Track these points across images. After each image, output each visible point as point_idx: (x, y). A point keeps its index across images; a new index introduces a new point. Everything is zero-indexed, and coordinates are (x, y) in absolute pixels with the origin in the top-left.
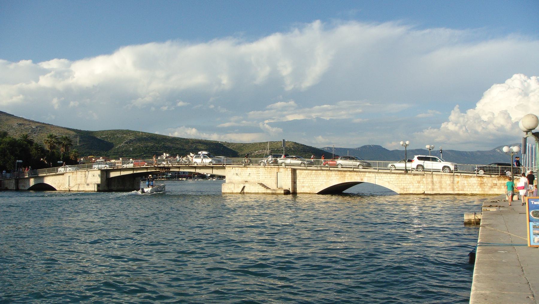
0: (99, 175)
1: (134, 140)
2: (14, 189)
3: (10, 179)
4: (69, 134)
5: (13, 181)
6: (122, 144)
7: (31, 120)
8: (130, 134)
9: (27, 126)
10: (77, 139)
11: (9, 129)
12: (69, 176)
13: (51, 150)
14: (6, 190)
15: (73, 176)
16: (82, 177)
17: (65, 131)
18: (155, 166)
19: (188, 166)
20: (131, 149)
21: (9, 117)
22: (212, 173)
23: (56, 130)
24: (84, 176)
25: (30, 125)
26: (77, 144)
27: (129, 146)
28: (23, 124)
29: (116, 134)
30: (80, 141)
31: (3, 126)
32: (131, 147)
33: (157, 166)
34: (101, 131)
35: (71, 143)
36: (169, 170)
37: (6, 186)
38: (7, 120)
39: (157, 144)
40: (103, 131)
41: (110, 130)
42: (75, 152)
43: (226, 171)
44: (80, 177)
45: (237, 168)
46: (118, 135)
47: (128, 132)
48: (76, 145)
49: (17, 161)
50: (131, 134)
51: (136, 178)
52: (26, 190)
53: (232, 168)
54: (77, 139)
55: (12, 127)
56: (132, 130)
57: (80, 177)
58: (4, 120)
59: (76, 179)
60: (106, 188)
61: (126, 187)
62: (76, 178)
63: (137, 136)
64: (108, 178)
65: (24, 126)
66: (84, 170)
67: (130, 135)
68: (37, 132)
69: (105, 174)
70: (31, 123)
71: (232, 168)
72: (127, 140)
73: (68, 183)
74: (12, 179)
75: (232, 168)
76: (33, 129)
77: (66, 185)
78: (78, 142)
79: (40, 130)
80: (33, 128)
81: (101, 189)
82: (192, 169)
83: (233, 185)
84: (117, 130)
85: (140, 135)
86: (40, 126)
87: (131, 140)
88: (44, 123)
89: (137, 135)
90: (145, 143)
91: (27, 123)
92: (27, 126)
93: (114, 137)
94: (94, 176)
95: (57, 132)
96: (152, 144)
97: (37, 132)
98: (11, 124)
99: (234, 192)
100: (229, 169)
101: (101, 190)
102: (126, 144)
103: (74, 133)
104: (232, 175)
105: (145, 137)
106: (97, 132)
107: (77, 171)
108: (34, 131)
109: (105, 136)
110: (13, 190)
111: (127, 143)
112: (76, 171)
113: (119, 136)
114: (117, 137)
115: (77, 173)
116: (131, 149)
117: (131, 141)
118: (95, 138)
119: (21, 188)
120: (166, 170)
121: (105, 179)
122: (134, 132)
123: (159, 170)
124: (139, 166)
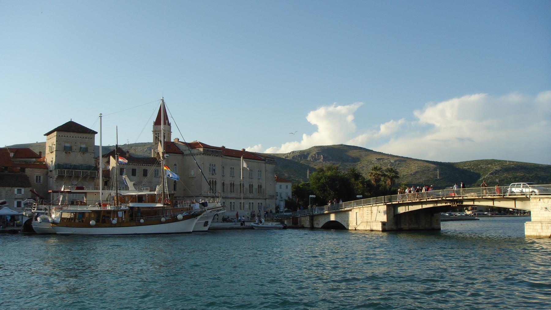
0: (384, 212)
1: (501, 170)
2: (309, 227)
3: (306, 216)
4: (429, 167)
5: (308, 218)
6: (487, 176)
7: (390, 154)
8: (495, 164)
9: (386, 161)
10: (437, 172)
11: (368, 165)
12: (356, 213)
13: (376, 183)
14: (303, 228)
15: (360, 212)
16: (369, 214)
17: (424, 164)
18: (443, 198)
19: (481, 197)
20: (497, 180)
21: (368, 152)
22: (514, 207)
23: (415, 163)
24: (370, 212)
25: (389, 160)
26: (437, 177)
27: (495, 178)
28: (382, 159)
29: (479, 165)
30: (440, 174)
31: (363, 162)
32: (497, 179)
33: (445, 199)
34: (462, 162)
35: (398, 175)
36: (462, 203)
37: (302, 224)
38: (366, 155)
39: (528, 174)
40: (465, 162)
41: (473, 161)
42: (405, 185)
43: (531, 203)
44: (367, 214)
45: (546, 200)
46: (482, 166)
47: (493, 162)
48: (436, 178)
49: (310, 196)
50: (496, 164)
51: (435, 215)
52: (190, 233)
53: (540, 200)
54: (437, 172)
55: (371, 162)
56: (497, 159)
57: (367, 214)
58: (363, 156)
59: (363, 217)
60: (394, 227)
61: (420, 226)
62: (363, 215)
63: (504, 166)
64: (395, 214)
65: (383, 161)
66: (370, 205)
67: (495, 165)
68: (396, 166)
69: (393, 209)
70: (390, 157)
71: (538, 199)
72: (492, 170)
73: (356, 221)
74: (307, 216)
75: (540, 200)
76: (392, 163)
77: (354, 223)
78: (438, 175)
79: (398, 164)
80: (392, 162)
81: (387, 228)
82: (470, 202)
83: (540, 224)
84: (481, 160)
85: (506, 165)
86: (398, 160)
87: (496, 170)
88: (402, 157)
89: (504, 164)
90: (513, 173)
91: (385, 157)
92: (386, 161)
93: (478, 168)
94: (546, 208)
95: (416, 165)
96: (522, 175)
97: (396, 166)
98: (370, 160)
99: (541, 235)
100: (535, 201)
101: (387, 229)
102: (491, 176)
103: (434, 166)
104: (540, 210)
105: (513, 167)
106: (458, 164)
107: (364, 206)
108: (393, 165)
109: (467, 168)
110: (308, 228)
111: (492, 174)
112: (362, 206)
113: (484, 166)
114: (481, 168)
115: (363, 209)
116: (497, 180)
117: (497, 172)
118: (458, 170)
119: (316, 226)
120: (458, 204)
121: (393, 215)
122: (499, 161)
123: (450, 204)
124: (411, 200)
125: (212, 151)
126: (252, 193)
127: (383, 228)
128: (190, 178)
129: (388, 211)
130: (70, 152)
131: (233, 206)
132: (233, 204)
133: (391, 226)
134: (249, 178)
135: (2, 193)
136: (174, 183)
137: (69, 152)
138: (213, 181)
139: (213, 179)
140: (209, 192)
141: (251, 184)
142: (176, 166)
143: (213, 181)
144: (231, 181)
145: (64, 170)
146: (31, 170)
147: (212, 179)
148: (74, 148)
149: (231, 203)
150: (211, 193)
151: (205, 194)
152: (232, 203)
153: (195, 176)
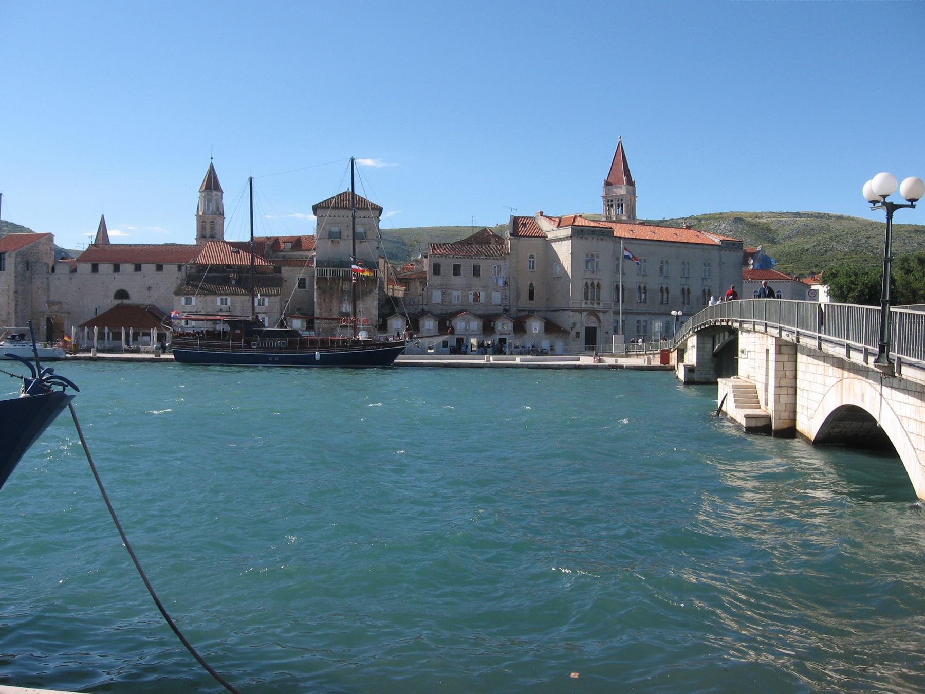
81: (696, 377)
125: (593, 231)
126: (688, 304)
127: (688, 379)
128: (554, 278)
129: (701, 346)
130: (339, 240)
131: (642, 327)
132: (645, 324)
133: (705, 374)
134: (681, 277)
135: (237, 305)
136: (530, 287)
137: (338, 241)
138: (592, 283)
139: (592, 279)
140: (583, 303)
141: (686, 288)
142: (533, 258)
143: (592, 283)
144: (640, 283)
145: (326, 269)
146: (290, 269)
147: (590, 280)
148: (369, 236)
149: (638, 322)
150: (589, 303)
151: (576, 306)
152: (642, 322)
153: (561, 276)
